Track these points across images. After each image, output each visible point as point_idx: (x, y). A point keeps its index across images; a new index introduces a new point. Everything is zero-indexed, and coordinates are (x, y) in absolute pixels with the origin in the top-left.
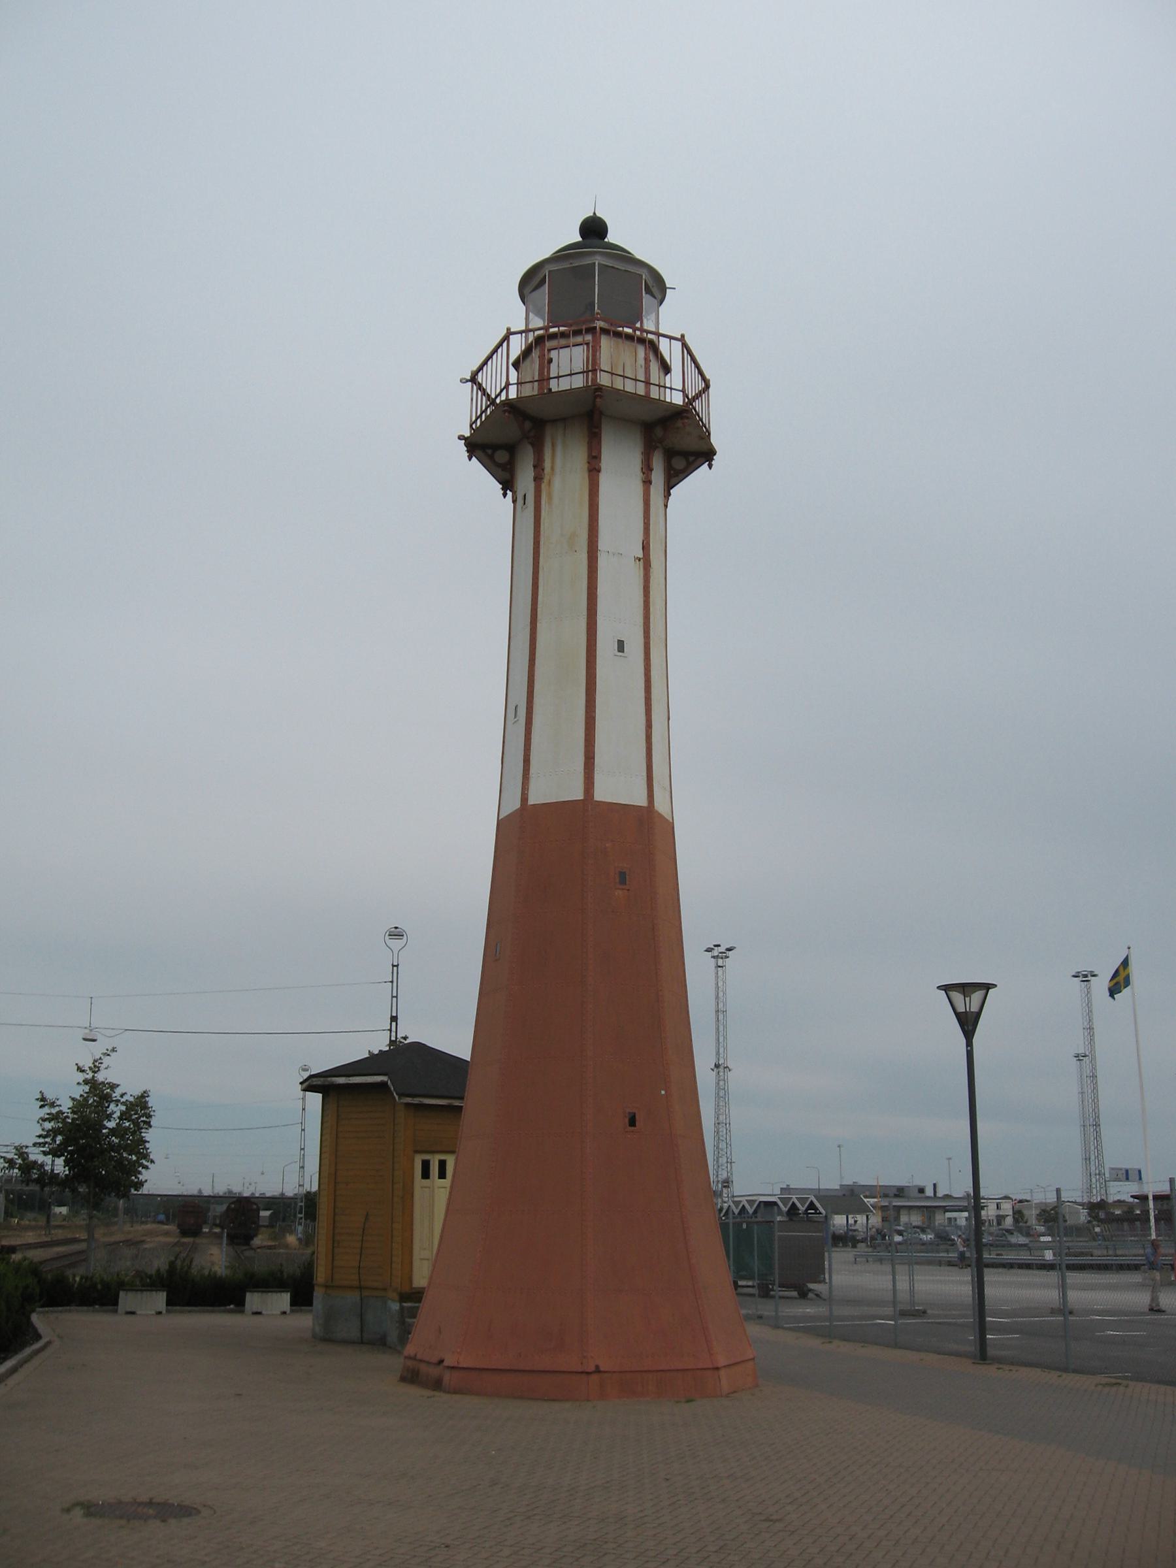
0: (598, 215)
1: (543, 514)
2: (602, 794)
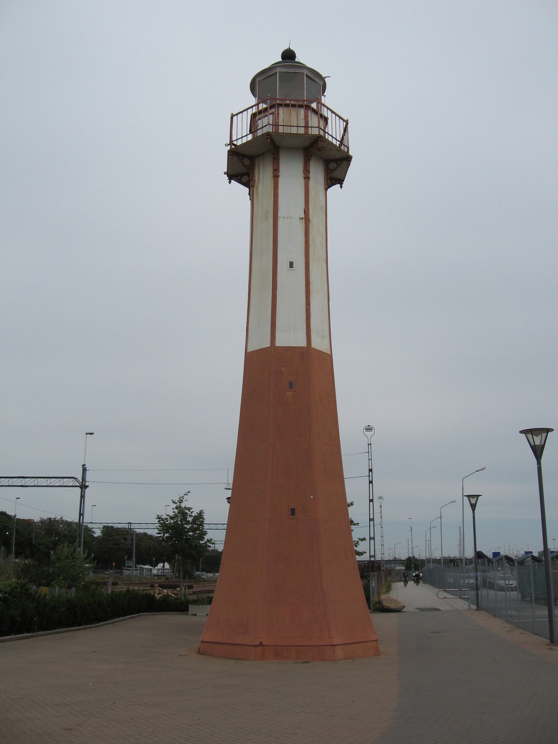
0: (291, 48)
1: (255, 203)
2: (280, 342)
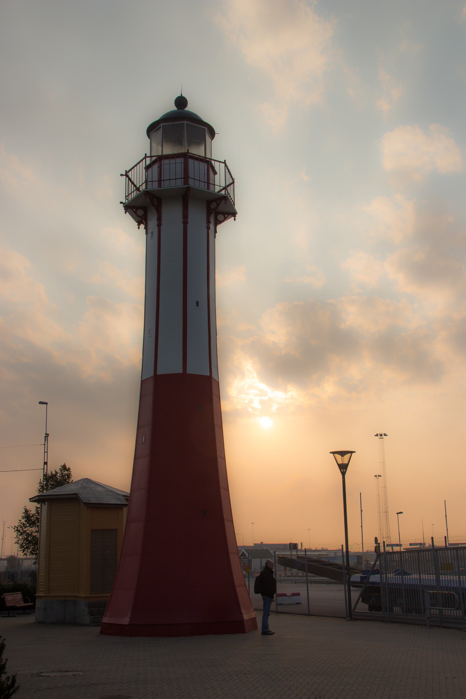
0: (183, 95)
